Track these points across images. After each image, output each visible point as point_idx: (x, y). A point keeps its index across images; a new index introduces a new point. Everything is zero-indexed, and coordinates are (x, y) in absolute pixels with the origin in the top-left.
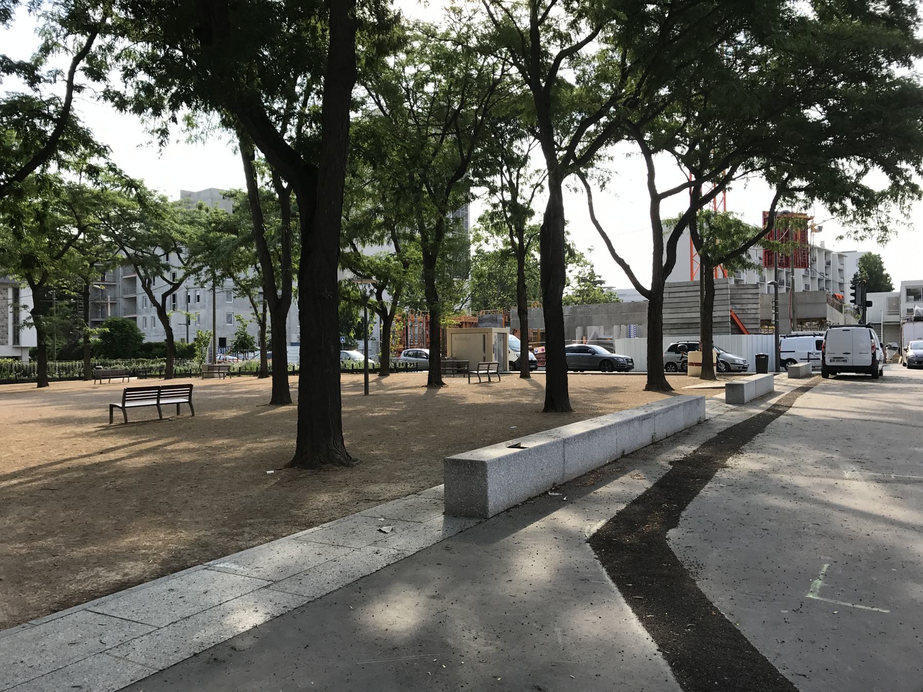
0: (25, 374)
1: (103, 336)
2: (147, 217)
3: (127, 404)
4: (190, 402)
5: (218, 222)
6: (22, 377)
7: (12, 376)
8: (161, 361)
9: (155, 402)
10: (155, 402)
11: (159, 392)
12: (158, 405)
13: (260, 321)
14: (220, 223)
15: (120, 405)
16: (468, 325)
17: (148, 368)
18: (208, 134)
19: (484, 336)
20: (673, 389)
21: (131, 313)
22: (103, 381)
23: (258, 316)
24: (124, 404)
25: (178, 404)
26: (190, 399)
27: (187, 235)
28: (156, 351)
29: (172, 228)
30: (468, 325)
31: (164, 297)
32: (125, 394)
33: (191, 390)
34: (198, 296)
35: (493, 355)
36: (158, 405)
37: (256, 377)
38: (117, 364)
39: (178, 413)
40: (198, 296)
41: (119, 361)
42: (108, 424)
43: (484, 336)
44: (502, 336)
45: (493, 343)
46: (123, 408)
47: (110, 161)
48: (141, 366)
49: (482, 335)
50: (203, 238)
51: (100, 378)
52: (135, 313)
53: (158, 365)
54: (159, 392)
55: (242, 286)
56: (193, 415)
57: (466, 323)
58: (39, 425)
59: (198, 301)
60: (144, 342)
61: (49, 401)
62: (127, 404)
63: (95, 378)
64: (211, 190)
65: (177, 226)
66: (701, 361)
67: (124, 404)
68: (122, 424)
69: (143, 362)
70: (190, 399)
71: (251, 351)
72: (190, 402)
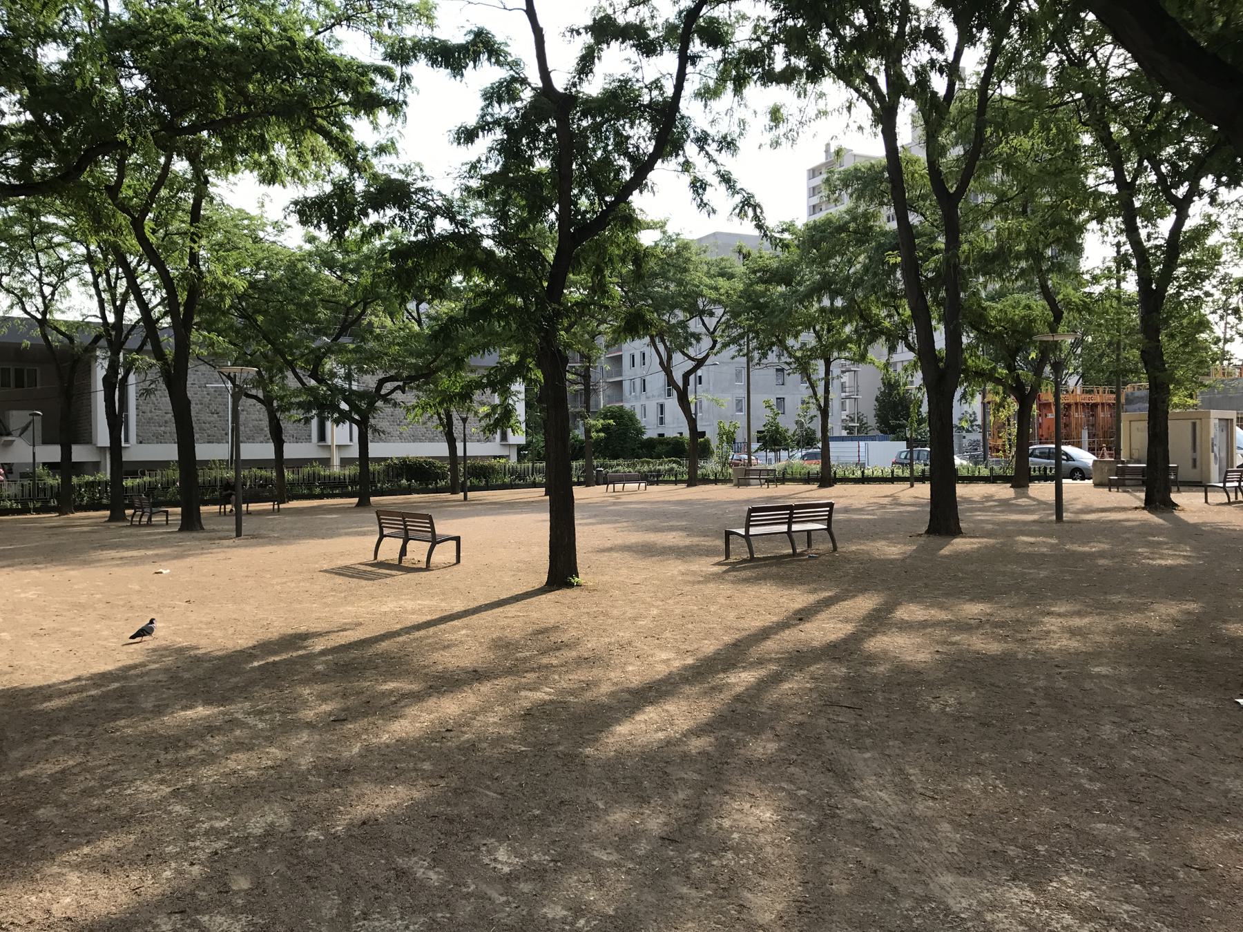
0: (520, 477)
1: (605, 429)
2: (669, 271)
3: (753, 531)
4: (829, 529)
5: (764, 270)
6: (517, 482)
7: (507, 480)
8: (670, 462)
9: (784, 528)
10: (784, 528)
11: (791, 514)
12: (789, 532)
13: (819, 406)
14: (767, 271)
15: (742, 531)
16: (1106, 408)
17: (654, 471)
18: (800, 130)
19: (1194, 424)
20: (1176, 505)
21: (617, 401)
22: (628, 486)
23: (817, 400)
24: (747, 531)
25: (809, 532)
26: (829, 525)
27: (722, 291)
28: (659, 449)
29: (701, 283)
30: (1106, 408)
31: (686, 377)
32: (749, 516)
33: (831, 512)
34: (700, 377)
35: (1212, 455)
36: (789, 532)
37: (815, 486)
38: (618, 465)
39: (809, 545)
40: (700, 377)
41: (621, 461)
42: (723, 558)
43: (1194, 424)
44: (1224, 423)
45: (1212, 435)
46: (747, 537)
47: (722, 168)
48: (646, 468)
49: (1189, 424)
50: (747, 294)
51: (613, 482)
52: (622, 401)
53: (667, 467)
54: (791, 514)
55: (797, 359)
56: (835, 548)
57: (1103, 404)
58: (626, 554)
59: (700, 383)
60: (645, 437)
61: (590, 517)
62: (753, 531)
63: (606, 483)
64: (714, 234)
65: (707, 281)
66: (242, 457)
67: (747, 531)
68: (744, 561)
69: (648, 463)
70: (829, 525)
71: (784, 449)
72: (829, 529)
